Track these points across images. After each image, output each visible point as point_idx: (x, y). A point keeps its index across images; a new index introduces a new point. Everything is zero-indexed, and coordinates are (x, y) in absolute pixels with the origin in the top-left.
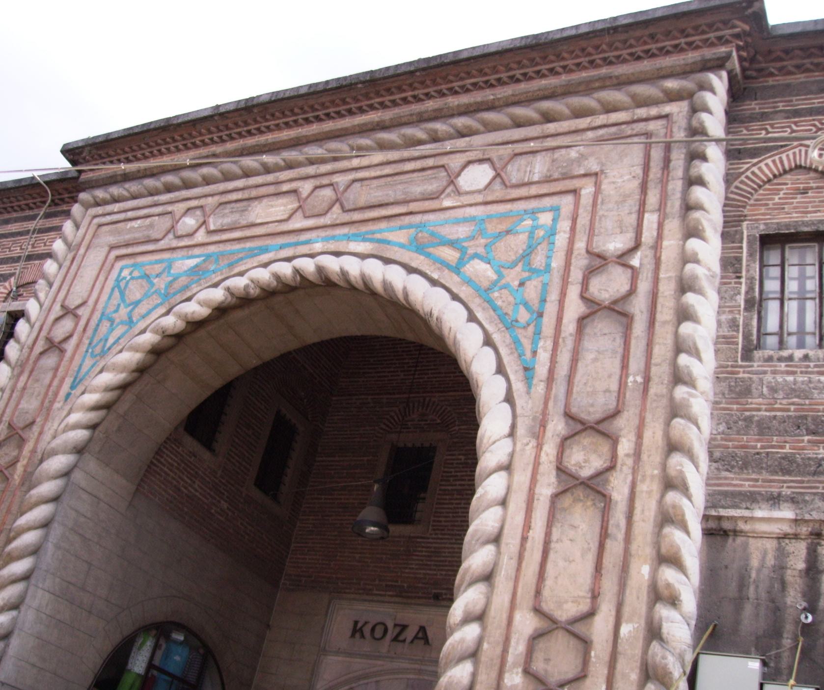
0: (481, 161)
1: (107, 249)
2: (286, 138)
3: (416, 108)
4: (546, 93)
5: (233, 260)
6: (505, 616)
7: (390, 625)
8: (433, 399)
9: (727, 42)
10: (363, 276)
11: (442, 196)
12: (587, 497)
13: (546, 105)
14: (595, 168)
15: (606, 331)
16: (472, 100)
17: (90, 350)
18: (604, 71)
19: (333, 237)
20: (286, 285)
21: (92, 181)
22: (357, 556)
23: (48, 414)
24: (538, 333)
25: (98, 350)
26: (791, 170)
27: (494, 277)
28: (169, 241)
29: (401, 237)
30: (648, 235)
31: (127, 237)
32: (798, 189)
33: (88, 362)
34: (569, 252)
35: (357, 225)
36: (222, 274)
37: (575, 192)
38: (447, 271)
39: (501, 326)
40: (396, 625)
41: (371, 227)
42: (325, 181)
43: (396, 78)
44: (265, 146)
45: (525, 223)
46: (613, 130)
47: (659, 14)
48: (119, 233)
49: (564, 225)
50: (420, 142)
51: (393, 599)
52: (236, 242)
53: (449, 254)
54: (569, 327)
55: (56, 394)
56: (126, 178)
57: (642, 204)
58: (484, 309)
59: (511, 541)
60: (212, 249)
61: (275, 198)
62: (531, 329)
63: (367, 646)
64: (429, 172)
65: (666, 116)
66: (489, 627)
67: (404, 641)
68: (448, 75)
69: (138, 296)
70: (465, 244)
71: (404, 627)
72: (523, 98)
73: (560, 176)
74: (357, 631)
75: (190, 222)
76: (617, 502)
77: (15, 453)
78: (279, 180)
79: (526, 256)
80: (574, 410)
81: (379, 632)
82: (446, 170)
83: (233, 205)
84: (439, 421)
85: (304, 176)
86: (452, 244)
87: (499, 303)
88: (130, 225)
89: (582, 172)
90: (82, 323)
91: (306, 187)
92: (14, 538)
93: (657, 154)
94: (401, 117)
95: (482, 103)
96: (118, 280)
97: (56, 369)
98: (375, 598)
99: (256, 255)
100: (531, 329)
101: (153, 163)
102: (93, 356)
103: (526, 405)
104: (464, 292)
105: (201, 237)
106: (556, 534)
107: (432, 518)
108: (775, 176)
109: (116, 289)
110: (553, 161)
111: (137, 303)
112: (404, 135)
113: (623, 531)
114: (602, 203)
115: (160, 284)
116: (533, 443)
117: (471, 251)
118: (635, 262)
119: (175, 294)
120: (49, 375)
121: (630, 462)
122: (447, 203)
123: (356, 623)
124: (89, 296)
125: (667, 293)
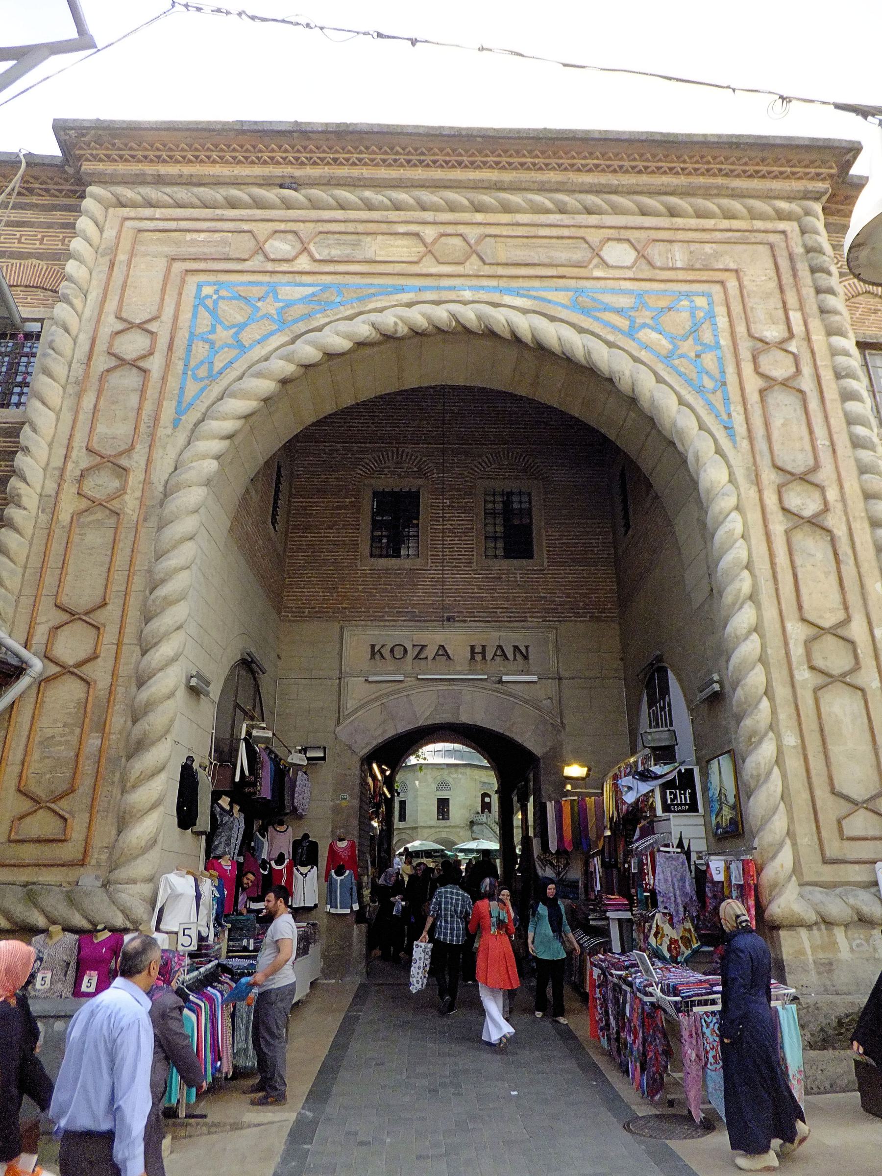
0: (619, 240)
1: (162, 263)
2: (386, 176)
3: (539, 176)
4: (668, 190)
5: (361, 295)
6: (778, 625)
7: (409, 648)
8: (406, 450)
9: (824, 179)
10: (479, 318)
11: (591, 266)
12: (815, 532)
13: (673, 200)
14: (732, 266)
15: (787, 403)
16: (596, 181)
17: (190, 373)
18: (720, 181)
19: (482, 288)
20: (439, 330)
21: (105, 174)
22: (360, 588)
23: (153, 440)
24: (726, 399)
25: (202, 372)
26: (863, 293)
27: (671, 347)
28: (256, 263)
29: (561, 297)
30: (798, 327)
31: (192, 250)
32: (871, 309)
33: (192, 388)
34: (733, 334)
35: (505, 279)
36: (353, 308)
37: (722, 283)
38: (620, 336)
39: (690, 389)
40: (414, 646)
41: (521, 283)
42: (450, 229)
43: (518, 141)
44: (360, 179)
45: (682, 303)
46: (738, 234)
47: (778, 142)
48: (177, 243)
49: (721, 310)
50: (548, 211)
51: (406, 623)
52: (359, 276)
53: (623, 323)
54: (753, 397)
55: (156, 419)
56: (217, 183)
57: (784, 303)
58: (669, 373)
59: (762, 567)
60: (328, 279)
61: (392, 237)
62: (719, 393)
63: (390, 665)
64: (568, 241)
65: (784, 232)
66: (768, 635)
67: (426, 658)
68: (571, 150)
69: (240, 318)
70: (632, 314)
71: (423, 647)
72: (646, 189)
73: (701, 267)
74: (375, 652)
75: (281, 247)
76: (839, 537)
77: (116, 484)
78: (389, 220)
79: (694, 331)
80: (780, 464)
81: (398, 653)
82: (587, 242)
83: (336, 236)
84: (415, 469)
85: (420, 220)
86: (619, 311)
87: (683, 369)
88: (189, 236)
89: (721, 267)
90: (162, 342)
91: (429, 233)
92: (163, 581)
93: (784, 264)
94: (521, 182)
95: (605, 186)
96: (200, 301)
97: (143, 391)
98: (387, 624)
99: (391, 293)
100: (719, 393)
101: (366, 172)
102: (195, 377)
103: (739, 460)
104: (643, 355)
105: (303, 263)
106: (798, 562)
107: (430, 553)
108: (853, 296)
109: (200, 307)
110: (691, 252)
111: (242, 327)
112: (531, 200)
113: (852, 558)
114: (749, 297)
115: (269, 307)
116: (754, 489)
117: (639, 321)
118: (793, 347)
119: (296, 321)
120: (134, 400)
121: (839, 506)
122: (597, 273)
123: (373, 647)
124: (160, 309)
125: (828, 378)
